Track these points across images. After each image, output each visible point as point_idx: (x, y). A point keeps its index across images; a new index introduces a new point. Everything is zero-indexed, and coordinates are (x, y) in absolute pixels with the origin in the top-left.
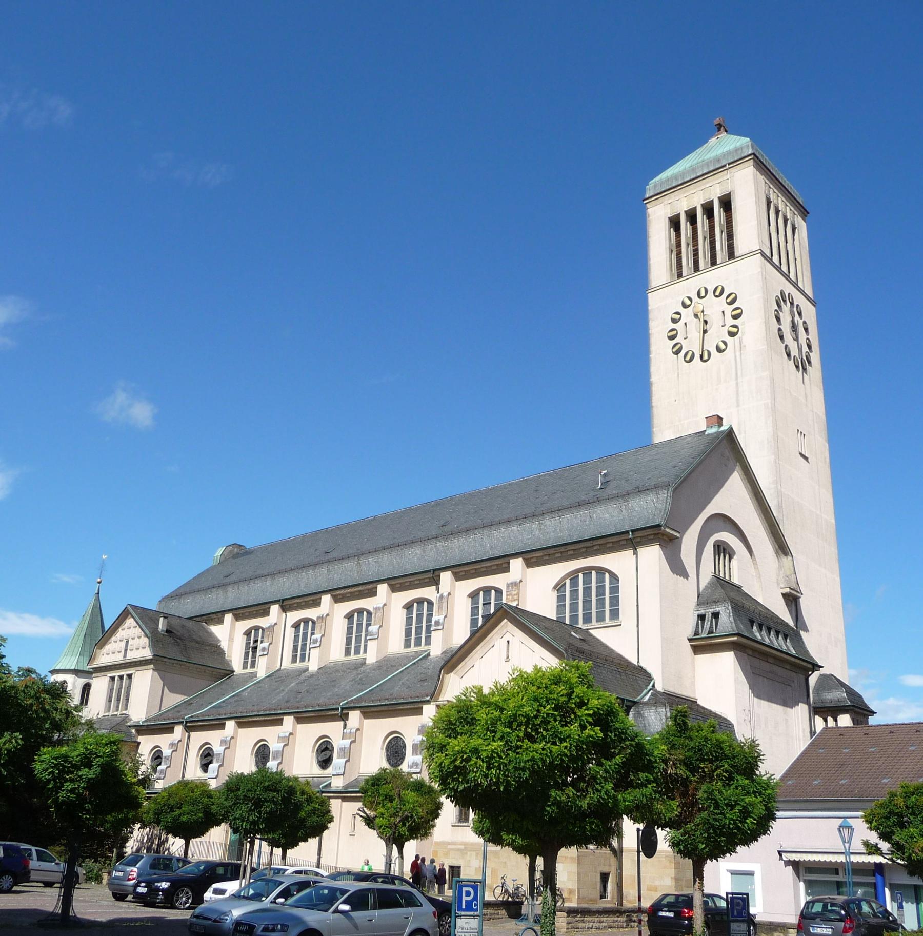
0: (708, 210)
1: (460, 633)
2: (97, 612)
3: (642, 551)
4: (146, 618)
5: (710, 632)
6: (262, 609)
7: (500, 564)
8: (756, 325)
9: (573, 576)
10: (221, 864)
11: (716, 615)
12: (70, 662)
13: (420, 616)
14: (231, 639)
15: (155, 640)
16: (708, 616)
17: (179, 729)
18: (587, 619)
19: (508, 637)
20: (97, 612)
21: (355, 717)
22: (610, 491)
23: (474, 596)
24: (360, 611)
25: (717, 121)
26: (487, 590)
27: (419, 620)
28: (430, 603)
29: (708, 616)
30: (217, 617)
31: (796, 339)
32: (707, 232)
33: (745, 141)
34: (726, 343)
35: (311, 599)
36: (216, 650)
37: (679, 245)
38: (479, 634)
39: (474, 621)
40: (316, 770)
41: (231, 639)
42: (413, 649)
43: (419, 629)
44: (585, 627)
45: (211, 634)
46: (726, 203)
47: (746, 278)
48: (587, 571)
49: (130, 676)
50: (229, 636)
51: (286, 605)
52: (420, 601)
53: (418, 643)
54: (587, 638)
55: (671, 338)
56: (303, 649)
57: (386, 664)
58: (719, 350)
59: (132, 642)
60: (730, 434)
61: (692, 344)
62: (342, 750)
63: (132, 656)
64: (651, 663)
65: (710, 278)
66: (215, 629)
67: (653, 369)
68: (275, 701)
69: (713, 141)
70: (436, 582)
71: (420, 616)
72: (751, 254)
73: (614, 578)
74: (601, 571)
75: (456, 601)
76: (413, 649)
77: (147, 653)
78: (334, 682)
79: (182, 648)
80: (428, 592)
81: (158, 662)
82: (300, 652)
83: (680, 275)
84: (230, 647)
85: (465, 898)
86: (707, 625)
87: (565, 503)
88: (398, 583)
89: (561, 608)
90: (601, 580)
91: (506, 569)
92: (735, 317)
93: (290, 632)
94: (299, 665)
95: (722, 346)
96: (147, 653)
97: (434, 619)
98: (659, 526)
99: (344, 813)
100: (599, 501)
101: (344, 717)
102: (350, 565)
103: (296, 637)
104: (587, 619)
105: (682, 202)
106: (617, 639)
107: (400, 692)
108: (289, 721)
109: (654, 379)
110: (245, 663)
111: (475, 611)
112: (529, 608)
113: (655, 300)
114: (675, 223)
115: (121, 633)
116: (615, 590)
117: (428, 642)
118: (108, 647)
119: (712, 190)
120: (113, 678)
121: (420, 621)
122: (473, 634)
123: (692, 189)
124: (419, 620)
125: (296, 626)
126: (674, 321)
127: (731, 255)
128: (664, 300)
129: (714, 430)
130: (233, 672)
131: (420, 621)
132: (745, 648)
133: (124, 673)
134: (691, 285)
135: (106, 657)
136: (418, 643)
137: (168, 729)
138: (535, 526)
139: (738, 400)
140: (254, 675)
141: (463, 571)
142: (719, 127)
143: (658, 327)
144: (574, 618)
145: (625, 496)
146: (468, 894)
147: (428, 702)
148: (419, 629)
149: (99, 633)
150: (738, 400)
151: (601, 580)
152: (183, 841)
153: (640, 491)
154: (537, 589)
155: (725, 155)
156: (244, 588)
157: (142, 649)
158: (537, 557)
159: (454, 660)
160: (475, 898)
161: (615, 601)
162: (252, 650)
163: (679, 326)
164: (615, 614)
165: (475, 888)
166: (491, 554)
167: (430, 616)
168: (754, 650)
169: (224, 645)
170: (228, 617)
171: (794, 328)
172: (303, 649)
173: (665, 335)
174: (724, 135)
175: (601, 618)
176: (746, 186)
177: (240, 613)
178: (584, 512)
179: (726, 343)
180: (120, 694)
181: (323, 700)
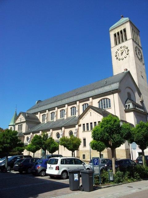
0: (121, 32)
1: (81, 112)
2: (16, 114)
3: (114, 94)
4: (24, 114)
5: (128, 108)
6: (45, 111)
7: (87, 99)
8: (132, 53)
9: (101, 100)
10: (106, 159)
11: (129, 105)
12: (12, 124)
13: (73, 110)
14: (40, 117)
15: (26, 118)
16: (128, 106)
17: (31, 133)
18: (105, 107)
19: (91, 111)
20: (16, 114)
21: (63, 128)
22: (107, 84)
23: (83, 105)
24: (63, 110)
25: (121, 16)
26: (85, 104)
27: (73, 110)
28: (75, 107)
29: (128, 106)
30: (37, 113)
31: (139, 55)
32: (121, 37)
33: (128, 18)
34: (124, 59)
35: (53, 108)
36: (38, 119)
37: (116, 39)
38: (85, 112)
39: (83, 110)
40: (57, 139)
41: (40, 117)
42: (73, 116)
43: (73, 112)
44: (104, 109)
45: (36, 116)
46: (125, 30)
47: (129, 44)
48: (104, 99)
49: (22, 125)
50: (39, 116)
51: (49, 110)
52: (73, 107)
53: (73, 115)
54: (105, 111)
55: (116, 56)
56: (53, 118)
57: (68, 119)
58: (125, 58)
59: (22, 118)
60: (129, 72)
61: (120, 57)
62: (61, 134)
63: (22, 121)
64: (118, 114)
65: (122, 44)
66: (37, 115)
67: (113, 62)
68: (49, 127)
69: (121, 19)
70: (76, 103)
71: (73, 110)
72: (130, 39)
73: (109, 100)
74: (107, 99)
75: (80, 107)
76: (73, 116)
77: (25, 120)
78: (59, 123)
79: (31, 120)
80: (75, 105)
81: (26, 122)
82: (52, 118)
83: (117, 44)
84: (40, 118)
85: (95, 162)
86: (128, 107)
87: (99, 87)
88: (69, 104)
89: (99, 106)
90: (107, 100)
91: (89, 100)
92: (128, 51)
93: (50, 115)
94: (52, 120)
95: (126, 57)
96: (25, 120)
97: (76, 110)
98: (117, 89)
99: (61, 148)
100: (105, 86)
101: (61, 129)
102: (60, 102)
103: (51, 115)
104: (105, 107)
105: (116, 31)
106: (111, 111)
107: (71, 123)
108: (51, 130)
109: (113, 64)
110: (43, 121)
111: (83, 108)
112: (93, 106)
113: (112, 49)
114: (115, 35)
115: (20, 117)
116: (110, 102)
117: (75, 114)
118: (18, 120)
119: (122, 28)
120: (19, 125)
121: (73, 111)
122: (83, 112)
123: (118, 28)
124: (73, 110)
125: (51, 113)
126: (116, 53)
127: (126, 40)
128: (114, 49)
129: (126, 71)
130: (40, 123)
131: (73, 111)
132: (134, 110)
133: (21, 124)
134: (119, 46)
135: (17, 122)
136: (73, 115)
137: (29, 134)
138: (94, 91)
139: (129, 66)
140: (44, 123)
141: (81, 101)
142: (122, 17)
143: (113, 55)
144: (102, 107)
145: (110, 84)
146: (96, 161)
147: (77, 125)
148: (73, 112)
149: (17, 117)
150: (129, 66)
151: (107, 100)
152: (33, 153)
153: (113, 83)
154: (95, 103)
155: (124, 21)
156: (41, 107)
157: (24, 119)
158: (94, 97)
159: (81, 117)
160: (98, 162)
161: (110, 104)
162: (43, 120)
163: (117, 54)
164: (110, 106)
165: (97, 159)
166: (86, 97)
167: (75, 110)
168: (137, 111)
169: (39, 118)
170: (39, 113)
171: (139, 53)
172: (53, 118)
173: (115, 52)
174: (123, 18)
175: (107, 107)
176: (128, 27)
177: (41, 112)
178: (103, 88)
179: (124, 59)
180: (20, 128)
181: (57, 126)
